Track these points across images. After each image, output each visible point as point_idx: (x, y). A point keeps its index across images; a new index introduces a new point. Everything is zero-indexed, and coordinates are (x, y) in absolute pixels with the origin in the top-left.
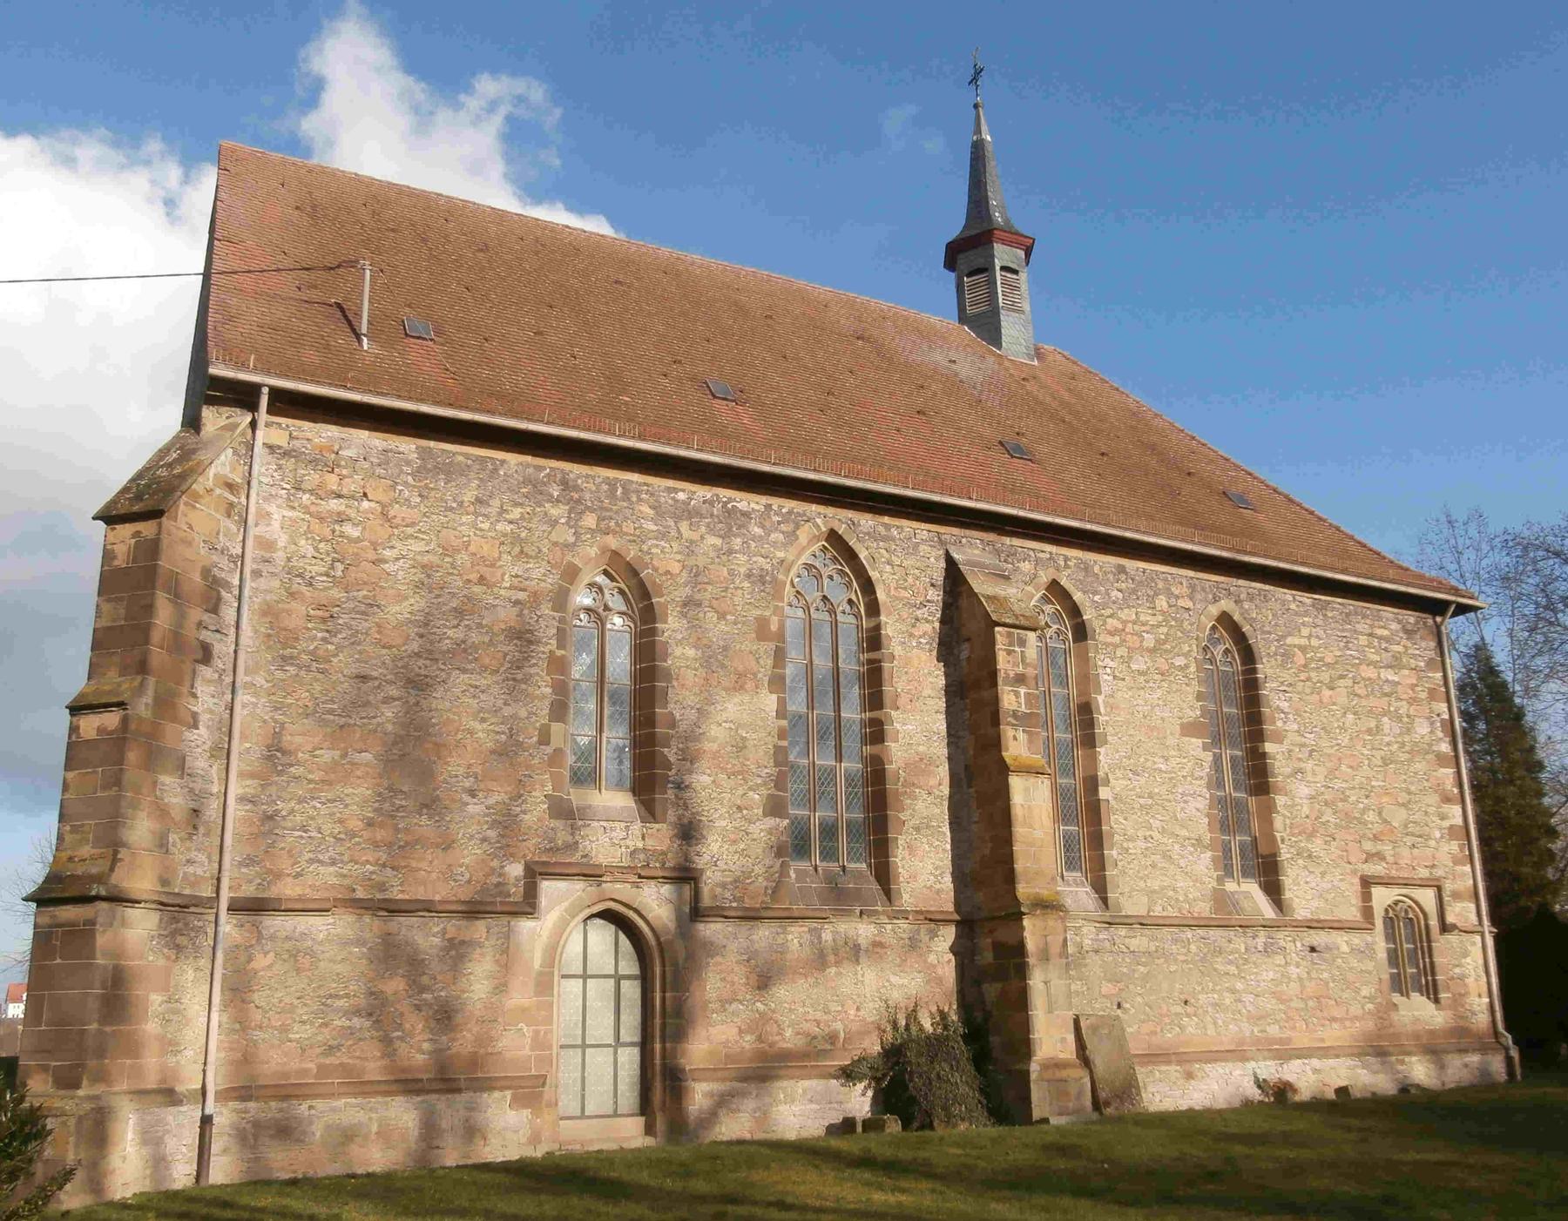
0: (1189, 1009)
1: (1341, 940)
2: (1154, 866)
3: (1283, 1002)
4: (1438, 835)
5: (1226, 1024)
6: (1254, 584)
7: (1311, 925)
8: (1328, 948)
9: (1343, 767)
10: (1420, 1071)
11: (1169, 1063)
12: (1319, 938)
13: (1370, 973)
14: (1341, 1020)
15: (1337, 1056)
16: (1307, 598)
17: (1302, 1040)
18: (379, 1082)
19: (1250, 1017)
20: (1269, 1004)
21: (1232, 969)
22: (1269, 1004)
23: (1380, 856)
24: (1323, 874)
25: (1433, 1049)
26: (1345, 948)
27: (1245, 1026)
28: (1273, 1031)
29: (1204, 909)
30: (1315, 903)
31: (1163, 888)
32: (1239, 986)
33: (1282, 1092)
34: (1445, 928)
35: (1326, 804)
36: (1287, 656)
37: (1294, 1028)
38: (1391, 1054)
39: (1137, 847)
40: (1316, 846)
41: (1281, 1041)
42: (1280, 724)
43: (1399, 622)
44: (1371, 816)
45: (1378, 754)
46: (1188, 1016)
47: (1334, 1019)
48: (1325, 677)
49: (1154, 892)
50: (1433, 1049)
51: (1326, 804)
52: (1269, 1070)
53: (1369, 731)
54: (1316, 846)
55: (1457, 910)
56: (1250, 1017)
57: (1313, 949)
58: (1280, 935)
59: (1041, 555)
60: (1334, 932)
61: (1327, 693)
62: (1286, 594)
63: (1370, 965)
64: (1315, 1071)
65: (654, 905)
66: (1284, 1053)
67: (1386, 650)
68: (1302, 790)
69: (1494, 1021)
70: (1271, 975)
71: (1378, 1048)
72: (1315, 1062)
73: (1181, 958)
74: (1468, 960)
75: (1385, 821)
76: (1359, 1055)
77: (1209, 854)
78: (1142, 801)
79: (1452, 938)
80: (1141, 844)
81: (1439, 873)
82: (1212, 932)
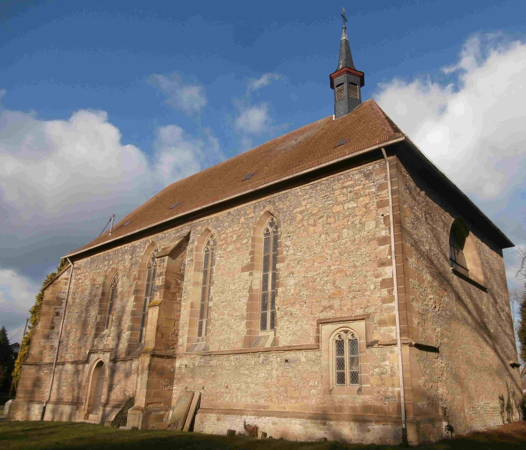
0: (228, 390)
1: (302, 356)
2: (223, 330)
3: (267, 387)
4: (372, 287)
5: (242, 397)
6: (281, 193)
7: (289, 349)
8: (295, 361)
9: (316, 264)
10: (348, 431)
11: (212, 413)
12: (289, 355)
13: (316, 372)
14: (297, 398)
15: (286, 417)
16: (307, 187)
17: (274, 407)
18: (109, 396)
19: (252, 395)
20: (262, 389)
21: (246, 372)
22: (262, 389)
23: (331, 307)
24: (296, 322)
25: (361, 419)
26: (303, 359)
27: (249, 399)
28: (262, 402)
29: (239, 346)
30: (290, 338)
31: (225, 339)
32: (249, 380)
33: (253, 430)
34: (370, 345)
35: (303, 285)
36: (293, 219)
37: (271, 401)
38: (330, 420)
39: (217, 324)
40: (294, 310)
41: (264, 407)
42: (285, 253)
43: (361, 172)
44: (329, 286)
45: (337, 252)
46: (226, 393)
47: (292, 398)
48: (311, 221)
49: (222, 341)
50: (361, 419)
51: (303, 285)
52: (251, 420)
53: (333, 241)
54: (294, 310)
55: (382, 331)
56: (252, 395)
57: (287, 361)
58: (271, 355)
59: (204, 222)
60: (298, 352)
61: (312, 229)
62: (297, 190)
63: (316, 369)
64: (274, 423)
65: (406, 236)
66: (260, 412)
67: (350, 192)
68: (291, 281)
69: (230, 412)
70: (263, 375)
71: (322, 417)
72: (275, 419)
73: (228, 368)
74: (387, 363)
75: (336, 287)
76: (310, 418)
77: (245, 321)
78: (223, 304)
79: (375, 350)
80: (220, 322)
81: (371, 310)
82: (241, 356)
